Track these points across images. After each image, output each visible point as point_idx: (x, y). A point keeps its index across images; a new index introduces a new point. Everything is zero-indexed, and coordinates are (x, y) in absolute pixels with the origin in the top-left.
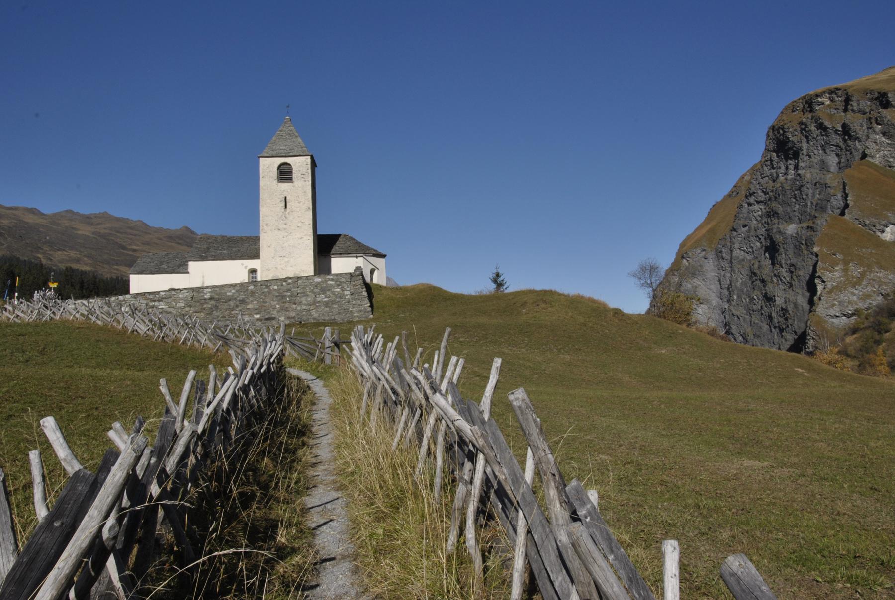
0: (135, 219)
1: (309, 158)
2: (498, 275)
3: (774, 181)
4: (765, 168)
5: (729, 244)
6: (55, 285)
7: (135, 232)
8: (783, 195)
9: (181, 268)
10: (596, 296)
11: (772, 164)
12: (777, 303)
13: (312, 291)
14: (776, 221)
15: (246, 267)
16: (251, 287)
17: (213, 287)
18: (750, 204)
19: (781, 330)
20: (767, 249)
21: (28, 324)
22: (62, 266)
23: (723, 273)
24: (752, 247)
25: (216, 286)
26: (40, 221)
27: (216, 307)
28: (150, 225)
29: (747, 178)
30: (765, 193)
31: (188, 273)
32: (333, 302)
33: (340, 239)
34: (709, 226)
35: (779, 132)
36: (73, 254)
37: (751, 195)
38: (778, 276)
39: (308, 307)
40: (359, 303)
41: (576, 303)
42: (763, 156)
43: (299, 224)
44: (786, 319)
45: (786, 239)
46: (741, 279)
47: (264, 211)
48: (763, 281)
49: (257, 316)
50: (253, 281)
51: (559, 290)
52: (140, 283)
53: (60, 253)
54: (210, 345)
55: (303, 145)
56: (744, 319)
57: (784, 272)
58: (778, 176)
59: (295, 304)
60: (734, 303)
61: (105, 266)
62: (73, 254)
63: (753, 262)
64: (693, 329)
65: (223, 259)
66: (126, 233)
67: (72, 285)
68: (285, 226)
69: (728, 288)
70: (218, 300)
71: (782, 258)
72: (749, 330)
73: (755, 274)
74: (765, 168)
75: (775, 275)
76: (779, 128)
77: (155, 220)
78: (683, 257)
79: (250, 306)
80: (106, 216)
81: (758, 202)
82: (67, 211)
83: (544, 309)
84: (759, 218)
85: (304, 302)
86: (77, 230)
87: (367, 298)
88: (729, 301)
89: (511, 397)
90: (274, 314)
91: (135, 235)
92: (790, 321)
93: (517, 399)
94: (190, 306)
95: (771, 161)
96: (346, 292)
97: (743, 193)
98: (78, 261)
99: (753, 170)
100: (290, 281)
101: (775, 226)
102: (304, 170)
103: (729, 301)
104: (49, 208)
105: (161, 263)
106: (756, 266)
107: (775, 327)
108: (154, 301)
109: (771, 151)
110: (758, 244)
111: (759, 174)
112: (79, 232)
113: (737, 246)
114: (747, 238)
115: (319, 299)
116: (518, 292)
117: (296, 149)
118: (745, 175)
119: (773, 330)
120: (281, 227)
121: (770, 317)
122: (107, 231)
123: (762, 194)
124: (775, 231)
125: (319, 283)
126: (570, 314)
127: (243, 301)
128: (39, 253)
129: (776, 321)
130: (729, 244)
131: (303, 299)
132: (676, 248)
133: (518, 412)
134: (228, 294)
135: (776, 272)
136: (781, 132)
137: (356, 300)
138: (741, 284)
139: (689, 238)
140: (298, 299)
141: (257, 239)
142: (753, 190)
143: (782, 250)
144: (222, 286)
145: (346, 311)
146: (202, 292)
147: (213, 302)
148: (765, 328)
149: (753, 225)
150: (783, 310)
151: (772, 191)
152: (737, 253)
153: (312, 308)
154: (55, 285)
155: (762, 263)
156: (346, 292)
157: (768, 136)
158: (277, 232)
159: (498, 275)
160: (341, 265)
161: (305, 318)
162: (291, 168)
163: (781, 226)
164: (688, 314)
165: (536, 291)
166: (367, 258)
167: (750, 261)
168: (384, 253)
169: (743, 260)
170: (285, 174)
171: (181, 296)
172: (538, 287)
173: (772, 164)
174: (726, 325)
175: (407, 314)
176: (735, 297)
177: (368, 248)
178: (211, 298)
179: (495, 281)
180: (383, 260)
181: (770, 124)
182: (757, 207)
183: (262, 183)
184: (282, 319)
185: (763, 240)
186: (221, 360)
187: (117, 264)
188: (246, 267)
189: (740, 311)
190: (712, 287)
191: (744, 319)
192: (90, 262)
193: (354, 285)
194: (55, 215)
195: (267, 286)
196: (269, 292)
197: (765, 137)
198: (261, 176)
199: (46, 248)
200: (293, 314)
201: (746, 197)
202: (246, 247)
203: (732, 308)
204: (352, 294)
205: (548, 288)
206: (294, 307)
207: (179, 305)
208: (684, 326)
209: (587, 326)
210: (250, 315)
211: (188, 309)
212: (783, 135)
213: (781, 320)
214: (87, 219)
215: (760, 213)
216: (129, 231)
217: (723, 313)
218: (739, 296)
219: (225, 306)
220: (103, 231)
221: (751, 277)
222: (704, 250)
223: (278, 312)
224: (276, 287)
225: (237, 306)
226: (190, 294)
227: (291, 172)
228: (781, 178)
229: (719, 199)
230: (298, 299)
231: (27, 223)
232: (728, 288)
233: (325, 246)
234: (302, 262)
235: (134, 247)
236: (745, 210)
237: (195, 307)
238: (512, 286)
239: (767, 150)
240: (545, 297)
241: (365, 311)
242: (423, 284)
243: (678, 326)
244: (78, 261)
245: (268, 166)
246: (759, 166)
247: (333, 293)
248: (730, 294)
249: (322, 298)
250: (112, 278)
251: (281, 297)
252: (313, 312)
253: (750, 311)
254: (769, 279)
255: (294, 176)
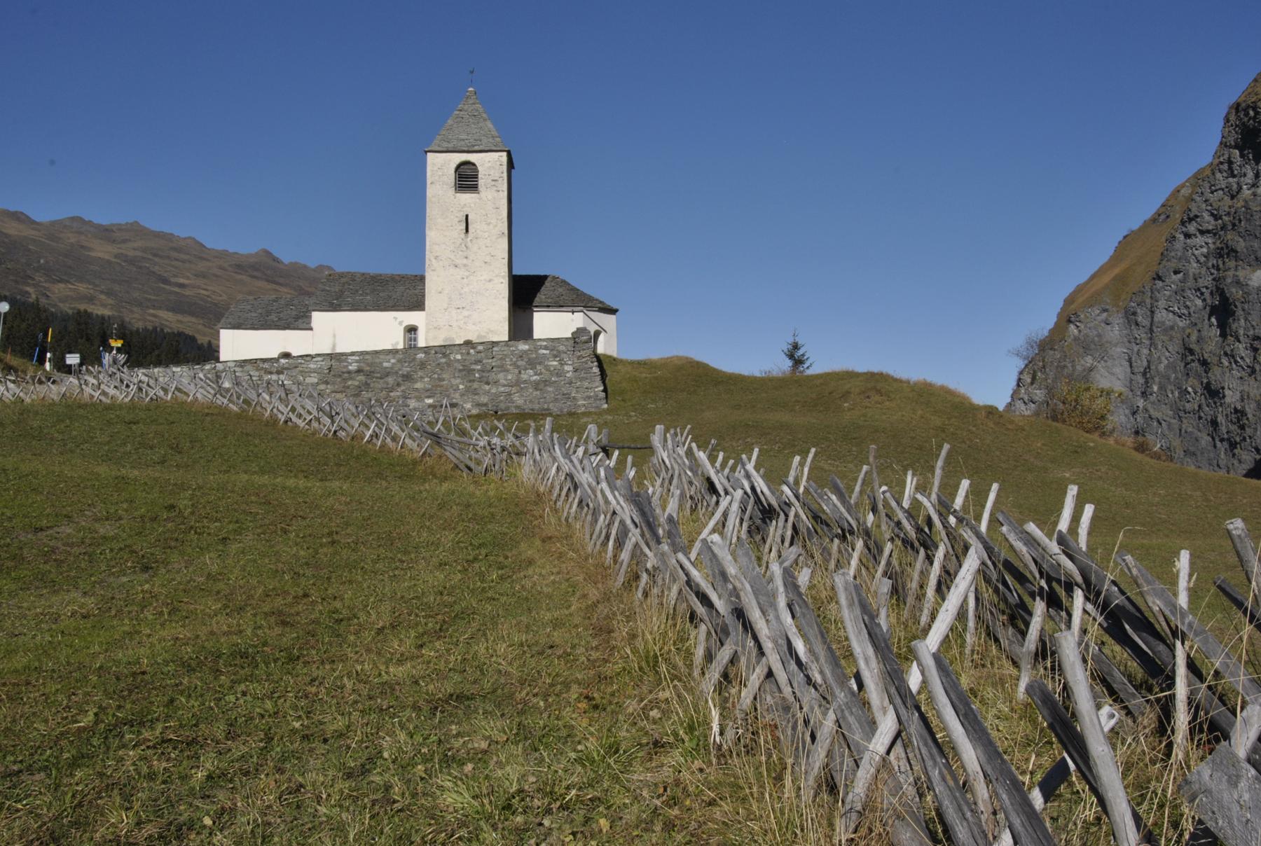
0: (183, 235)
1: (505, 154)
2: (796, 347)
3: (1233, 197)
4: (1218, 175)
5: (1148, 301)
6: (119, 344)
7: (183, 256)
8: (1248, 220)
9: (300, 321)
10: (952, 385)
11: (1230, 168)
12: (1228, 400)
13: (515, 365)
14: (1232, 264)
15: (401, 323)
16: (421, 356)
17: (362, 353)
18: (1187, 236)
19: (1233, 445)
20: (1214, 311)
21: (121, 407)
22: (67, 308)
23: (1136, 348)
24: (1187, 307)
25: (367, 353)
26: (27, 232)
27: (367, 384)
28: (208, 246)
29: (1185, 192)
30: (1216, 217)
31: (311, 329)
32: (546, 382)
33: (547, 283)
34: (1116, 271)
35: (1247, 114)
36: (82, 288)
37: (1190, 220)
38: (1231, 356)
39: (507, 389)
40: (586, 384)
41: (925, 394)
42: (1217, 155)
43: (488, 259)
44: (1242, 428)
45: (1248, 294)
46: (1166, 357)
47: (432, 235)
48: (1204, 363)
49: (430, 401)
50: (411, 347)
51: (891, 373)
52: (237, 345)
53: (62, 286)
54: (414, 445)
55: (495, 133)
56: (1169, 425)
57: (1242, 349)
58: (1240, 188)
59: (488, 383)
60: (1153, 398)
61: (135, 309)
62: (82, 288)
63: (1188, 331)
64: (1111, 441)
65: (366, 309)
66: (169, 257)
67: (88, 339)
68: (465, 261)
69: (1144, 374)
70: (369, 374)
71: (1239, 326)
72: (1176, 443)
73: (1191, 352)
74: (1218, 175)
75: (1226, 354)
76: (1248, 106)
77: (214, 241)
78: (1069, 321)
79: (418, 385)
80: (136, 230)
81: (1202, 232)
82: (73, 219)
83: (877, 402)
84: (1202, 259)
85: (503, 381)
86: (90, 249)
87: (599, 378)
88: (1144, 394)
89: (1231, 527)
90: (456, 398)
91: (184, 261)
92: (1249, 431)
93: (1236, 529)
94: (327, 383)
95: (1230, 162)
96: (567, 368)
97: (1176, 217)
98: (91, 299)
99: (1198, 179)
100: (480, 348)
101: (1230, 273)
102: (496, 175)
103: (1144, 394)
104: (44, 212)
105: (269, 313)
106: (1194, 338)
107: (1222, 440)
108: (271, 373)
109: (1231, 147)
110: (1199, 302)
111: (1207, 185)
112: (93, 254)
113: (1162, 304)
114: (1180, 292)
115: (524, 377)
116: (828, 374)
117: (485, 140)
118: (1183, 186)
119: (1219, 444)
120: (458, 262)
121: (1214, 423)
122: (138, 253)
123: (1211, 219)
124: (1229, 280)
125: (525, 352)
126: (920, 412)
127: (407, 377)
128: (28, 285)
129: (1224, 429)
130: (1148, 301)
131: (501, 376)
132: (1060, 304)
133: (1237, 540)
134: (385, 364)
135: (1228, 349)
136: (1252, 113)
137: (582, 379)
138: (1167, 367)
139: (1079, 289)
140: (492, 376)
141: (422, 279)
142: (1195, 211)
143: (1239, 312)
144: (376, 352)
145: (567, 396)
146: (345, 361)
147: (361, 378)
148: (1205, 440)
149: (1191, 272)
150: (1236, 411)
151: (1228, 214)
152: (1161, 315)
153: (514, 390)
154: (119, 344)
155: (1204, 333)
156: (567, 368)
157: (1227, 120)
158: (452, 270)
159: (796, 347)
160: (551, 324)
161: (502, 406)
162: (476, 170)
163: (1241, 274)
164: (1103, 417)
165: (858, 375)
166: (591, 314)
167: (1184, 329)
168: (615, 307)
169: (1172, 328)
170: (466, 179)
171: (312, 366)
172: (861, 367)
173: (1230, 168)
174: (1137, 433)
175: (660, 404)
176: (1155, 388)
177: (590, 299)
178: (359, 371)
179: (791, 356)
180: (612, 318)
181: (1233, 100)
182: (1200, 240)
183: (431, 191)
184: (468, 406)
185: (1207, 295)
186: (432, 468)
187: (154, 307)
188: (401, 323)
189: (1165, 412)
190: (1118, 370)
191: (1169, 425)
192: (110, 301)
193: (579, 358)
194: (53, 223)
195: (444, 355)
196: (449, 364)
197: (1221, 124)
198: (429, 182)
199: (39, 277)
200: (484, 399)
201: (1183, 223)
202: (404, 291)
203: (1149, 407)
204: (576, 370)
205: (876, 370)
206: (487, 387)
207: (308, 380)
208: (1095, 436)
209: (922, 425)
210: (419, 399)
211: (322, 387)
212: (1254, 118)
213: (1233, 428)
214: (106, 233)
215: (1205, 250)
216: (175, 254)
217: (1134, 413)
218: (1161, 388)
219: (381, 384)
220: (131, 254)
221: (1184, 357)
222: (1105, 310)
223: (462, 395)
224: (459, 357)
225: (398, 385)
226: (325, 364)
227: (476, 177)
228: (1246, 192)
229: (1136, 225)
230: (492, 376)
231: (6, 235)
232: (1144, 374)
233: (525, 293)
234: (492, 320)
235: (182, 281)
236: (1179, 245)
237: (334, 383)
238: (819, 364)
239: (1223, 144)
240: (877, 384)
241: (596, 398)
242: (679, 358)
243: (1088, 435)
244: (91, 299)
245: (441, 166)
246: (1208, 172)
247: (547, 368)
248: (1147, 382)
249: (529, 375)
250: (146, 330)
251: (467, 372)
252: (516, 397)
253: (1179, 413)
254: (1215, 360)
255: (481, 182)
